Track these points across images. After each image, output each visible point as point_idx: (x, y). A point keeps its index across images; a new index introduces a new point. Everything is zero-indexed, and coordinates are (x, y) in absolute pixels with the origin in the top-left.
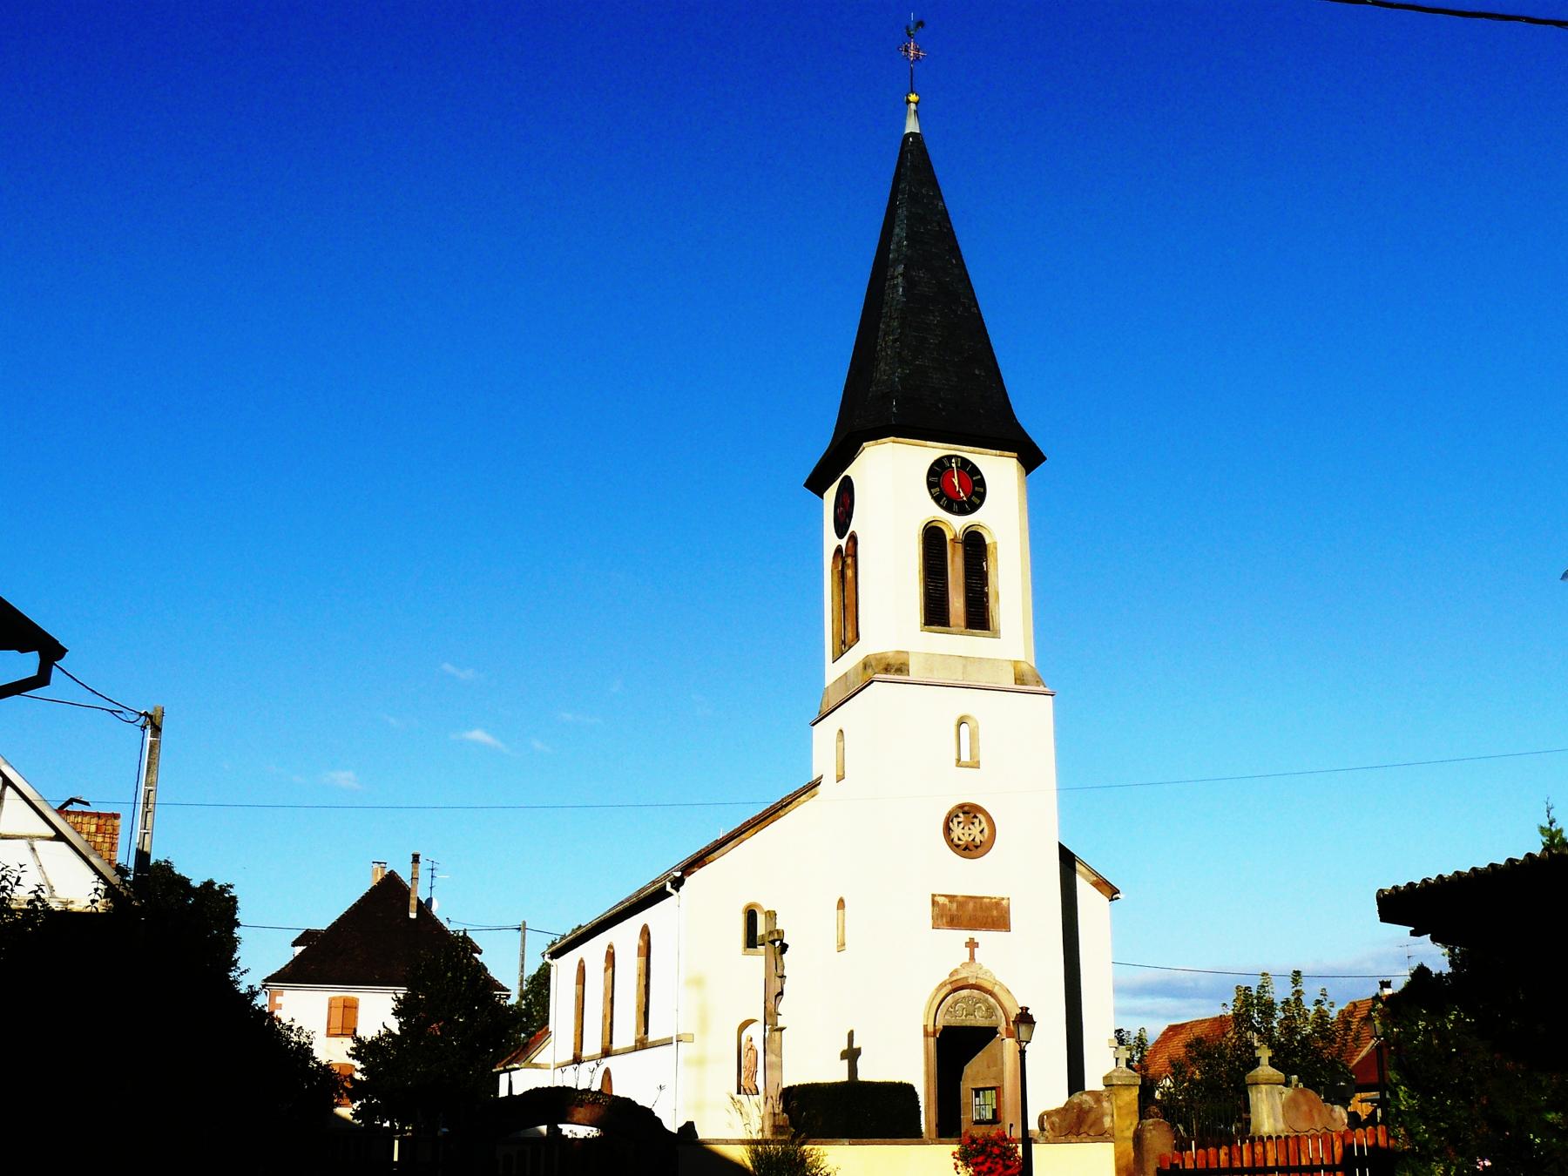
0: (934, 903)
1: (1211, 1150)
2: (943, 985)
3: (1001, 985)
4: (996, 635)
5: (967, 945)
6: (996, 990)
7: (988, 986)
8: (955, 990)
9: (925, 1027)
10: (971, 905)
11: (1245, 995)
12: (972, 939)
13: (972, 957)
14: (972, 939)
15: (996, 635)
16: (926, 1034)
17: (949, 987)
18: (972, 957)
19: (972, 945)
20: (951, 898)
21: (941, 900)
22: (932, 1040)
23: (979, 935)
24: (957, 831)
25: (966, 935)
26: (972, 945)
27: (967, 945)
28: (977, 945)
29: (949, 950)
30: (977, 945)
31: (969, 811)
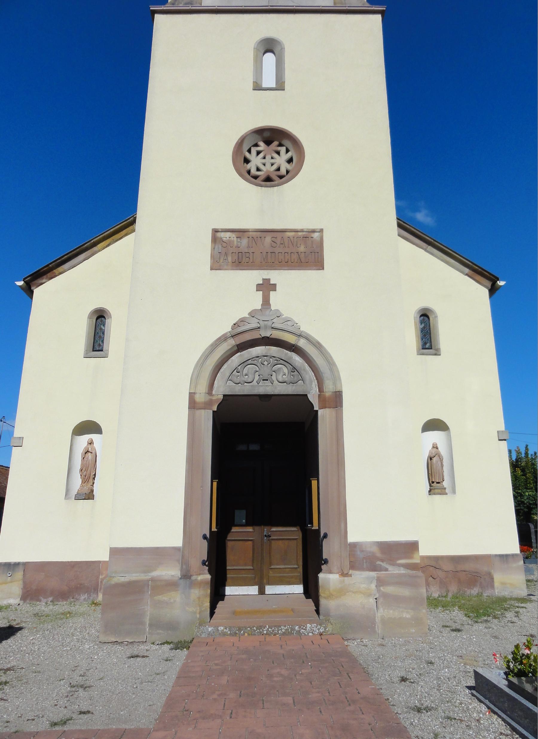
0: (215, 239)
1: (271, 574)
2: (223, 339)
3: (308, 338)
4: (437, 353)
5: (259, 287)
6: (302, 343)
7: (291, 339)
8: (242, 347)
9: (192, 395)
10: (268, 239)
11: (512, 653)
12: (266, 281)
13: (266, 302)
14: (266, 281)
15: (437, 353)
16: (193, 405)
17: (232, 342)
18: (266, 302)
19: (267, 287)
20: (240, 232)
21: (226, 236)
22: (206, 421)
23: (275, 276)
24: (256, 161)
25: (256, 276)
26: (267, 287)
27: (259, 287)
28: (274, 287)
29: (235, 297)
30: (274, 287)
31: (272, 137)
